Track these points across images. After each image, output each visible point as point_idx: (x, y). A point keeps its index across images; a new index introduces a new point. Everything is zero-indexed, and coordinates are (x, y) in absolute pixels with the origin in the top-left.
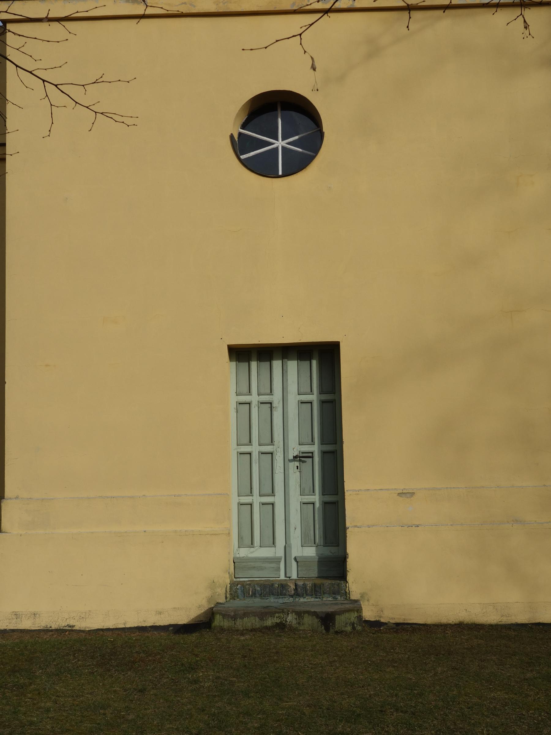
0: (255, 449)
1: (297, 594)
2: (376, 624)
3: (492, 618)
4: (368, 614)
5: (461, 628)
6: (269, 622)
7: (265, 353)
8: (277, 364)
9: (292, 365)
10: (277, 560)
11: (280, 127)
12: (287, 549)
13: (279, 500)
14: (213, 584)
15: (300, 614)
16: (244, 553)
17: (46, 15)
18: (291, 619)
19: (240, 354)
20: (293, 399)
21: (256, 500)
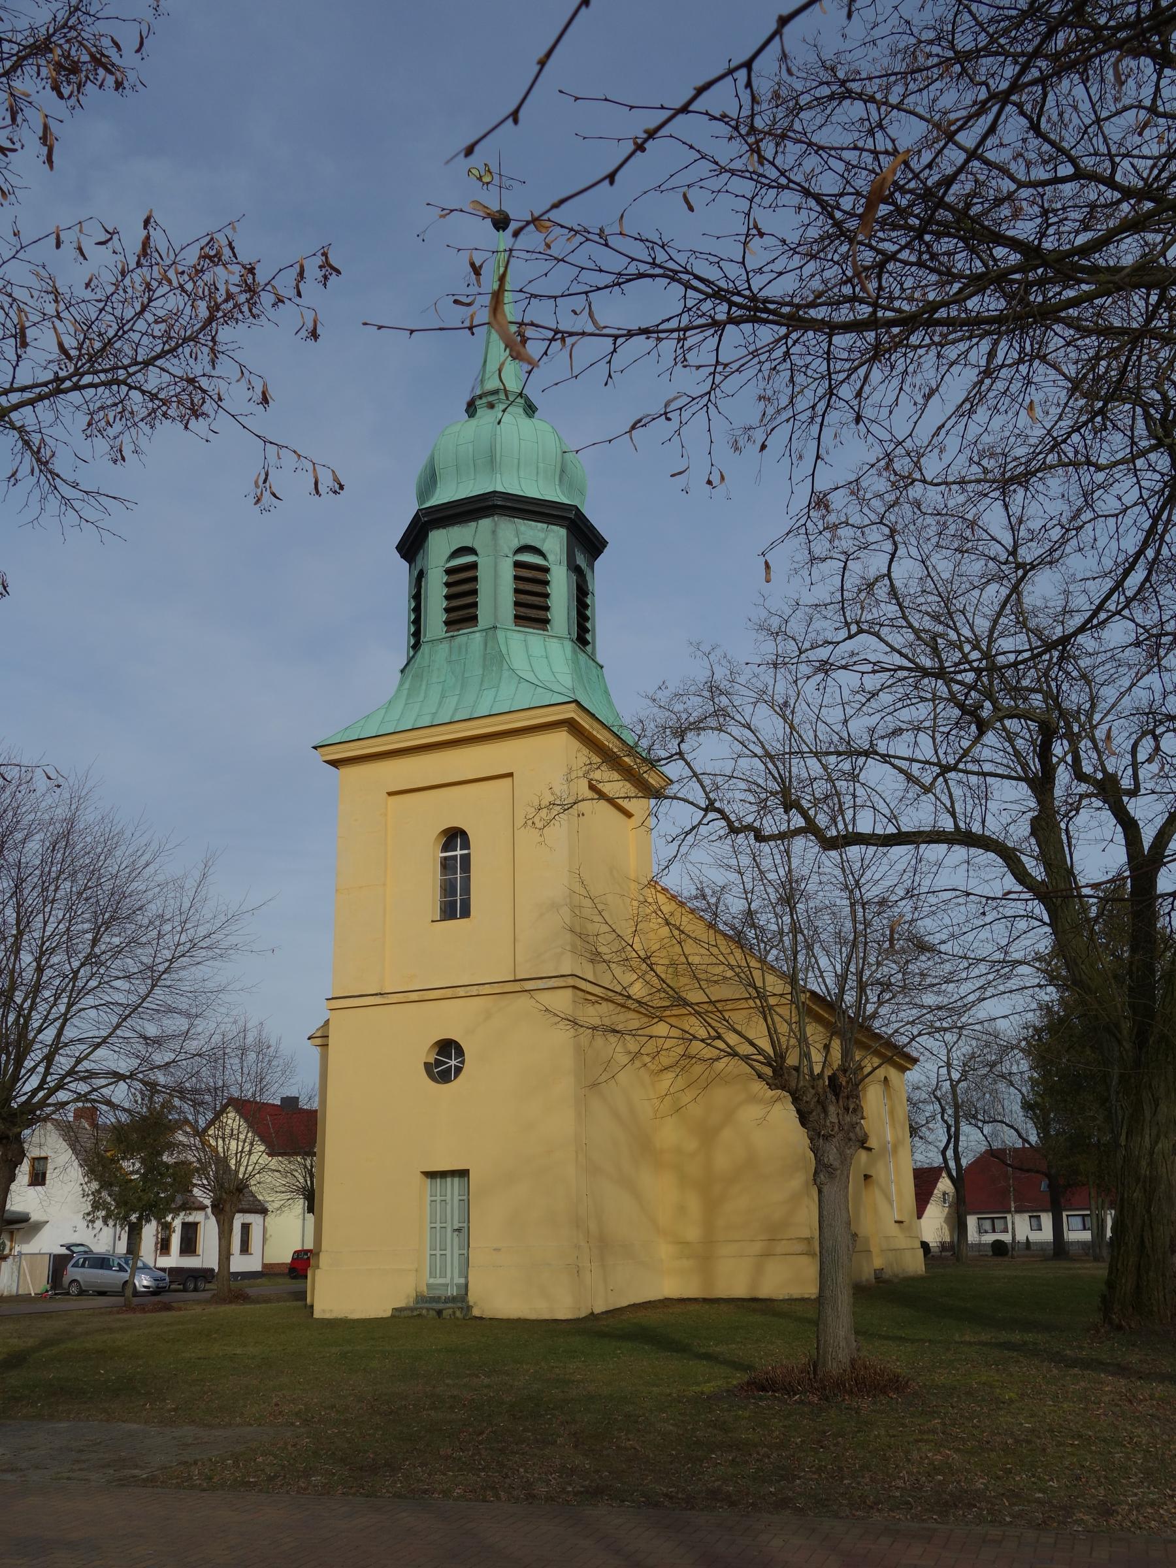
0: (438, 1225)
1: (446, 1302)
2: (481, 1318)
3: (533, 1316)
4: (476, 1312)
5: (519, 1320)
6: (415, 1313)
7: (443, 1174)
8: (449, 1180)
9: (456, 1180)
10: (447, 1285)
11: (446, 1059)
12: (452, 1278)
13: (448, 1252)
14: (408, 1297)
15: (428, 1309)
16: (432, 1281)
17: (784, 37)
18: (424, 1312)
19: (431, 1175)
20: (456, 1198)
21: (438, 1252)
